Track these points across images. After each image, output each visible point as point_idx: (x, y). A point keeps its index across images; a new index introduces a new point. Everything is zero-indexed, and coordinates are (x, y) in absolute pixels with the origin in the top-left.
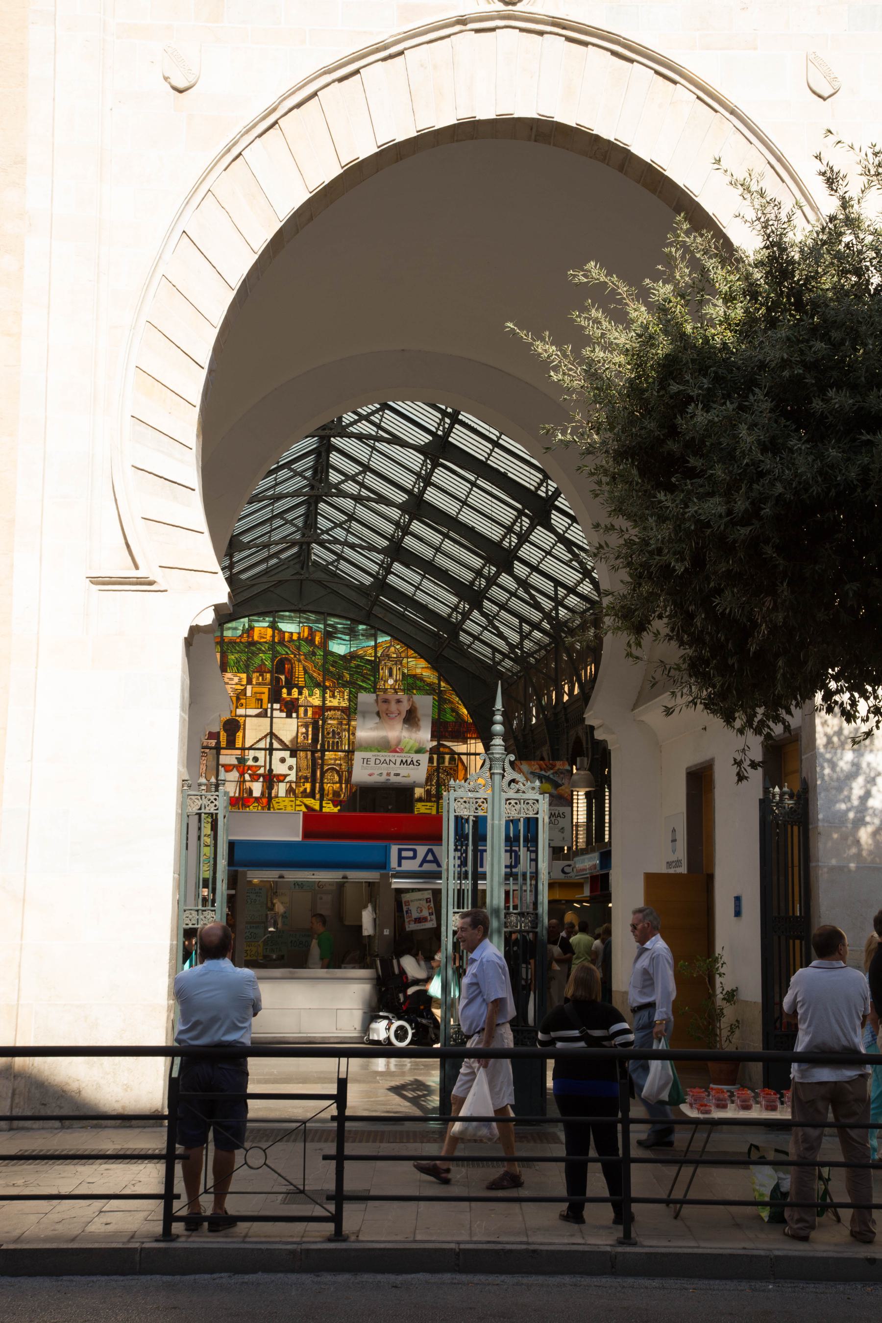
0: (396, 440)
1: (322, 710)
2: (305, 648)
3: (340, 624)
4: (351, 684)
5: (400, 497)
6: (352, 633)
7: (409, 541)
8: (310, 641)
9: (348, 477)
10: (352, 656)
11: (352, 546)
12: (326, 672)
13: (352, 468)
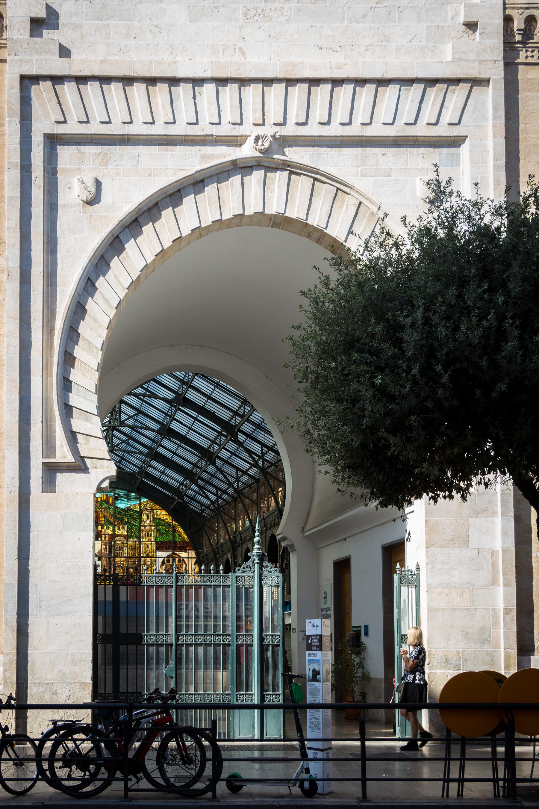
0: (148, 428)
1: (113, 537)
2: (105, 505)
3: (122, 493)
4: (128, 523)
5: (156, 426)
6: (128, 497)
7: (161, 450)
8: (107, 501)
9: (123, 441)
10: (128, 509)
11: (128, 452)
12: (115, 517)
13: (132, 412)
